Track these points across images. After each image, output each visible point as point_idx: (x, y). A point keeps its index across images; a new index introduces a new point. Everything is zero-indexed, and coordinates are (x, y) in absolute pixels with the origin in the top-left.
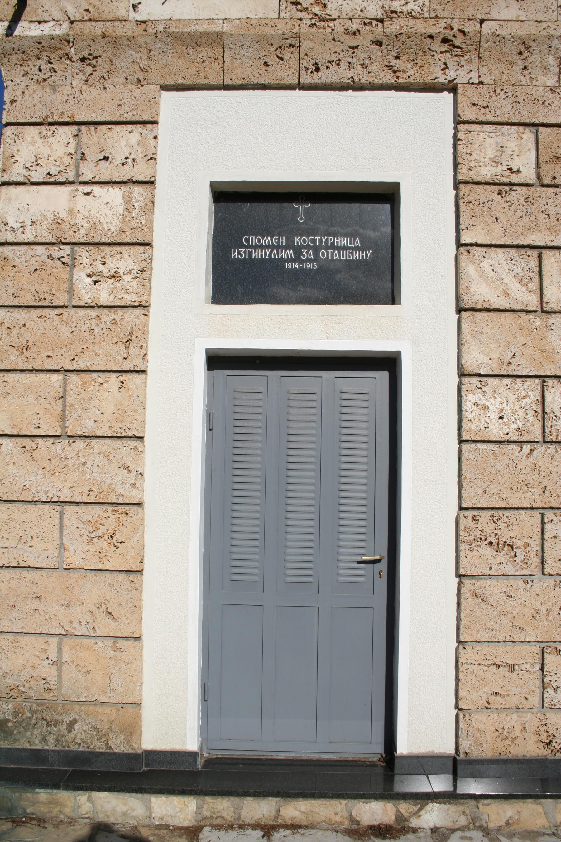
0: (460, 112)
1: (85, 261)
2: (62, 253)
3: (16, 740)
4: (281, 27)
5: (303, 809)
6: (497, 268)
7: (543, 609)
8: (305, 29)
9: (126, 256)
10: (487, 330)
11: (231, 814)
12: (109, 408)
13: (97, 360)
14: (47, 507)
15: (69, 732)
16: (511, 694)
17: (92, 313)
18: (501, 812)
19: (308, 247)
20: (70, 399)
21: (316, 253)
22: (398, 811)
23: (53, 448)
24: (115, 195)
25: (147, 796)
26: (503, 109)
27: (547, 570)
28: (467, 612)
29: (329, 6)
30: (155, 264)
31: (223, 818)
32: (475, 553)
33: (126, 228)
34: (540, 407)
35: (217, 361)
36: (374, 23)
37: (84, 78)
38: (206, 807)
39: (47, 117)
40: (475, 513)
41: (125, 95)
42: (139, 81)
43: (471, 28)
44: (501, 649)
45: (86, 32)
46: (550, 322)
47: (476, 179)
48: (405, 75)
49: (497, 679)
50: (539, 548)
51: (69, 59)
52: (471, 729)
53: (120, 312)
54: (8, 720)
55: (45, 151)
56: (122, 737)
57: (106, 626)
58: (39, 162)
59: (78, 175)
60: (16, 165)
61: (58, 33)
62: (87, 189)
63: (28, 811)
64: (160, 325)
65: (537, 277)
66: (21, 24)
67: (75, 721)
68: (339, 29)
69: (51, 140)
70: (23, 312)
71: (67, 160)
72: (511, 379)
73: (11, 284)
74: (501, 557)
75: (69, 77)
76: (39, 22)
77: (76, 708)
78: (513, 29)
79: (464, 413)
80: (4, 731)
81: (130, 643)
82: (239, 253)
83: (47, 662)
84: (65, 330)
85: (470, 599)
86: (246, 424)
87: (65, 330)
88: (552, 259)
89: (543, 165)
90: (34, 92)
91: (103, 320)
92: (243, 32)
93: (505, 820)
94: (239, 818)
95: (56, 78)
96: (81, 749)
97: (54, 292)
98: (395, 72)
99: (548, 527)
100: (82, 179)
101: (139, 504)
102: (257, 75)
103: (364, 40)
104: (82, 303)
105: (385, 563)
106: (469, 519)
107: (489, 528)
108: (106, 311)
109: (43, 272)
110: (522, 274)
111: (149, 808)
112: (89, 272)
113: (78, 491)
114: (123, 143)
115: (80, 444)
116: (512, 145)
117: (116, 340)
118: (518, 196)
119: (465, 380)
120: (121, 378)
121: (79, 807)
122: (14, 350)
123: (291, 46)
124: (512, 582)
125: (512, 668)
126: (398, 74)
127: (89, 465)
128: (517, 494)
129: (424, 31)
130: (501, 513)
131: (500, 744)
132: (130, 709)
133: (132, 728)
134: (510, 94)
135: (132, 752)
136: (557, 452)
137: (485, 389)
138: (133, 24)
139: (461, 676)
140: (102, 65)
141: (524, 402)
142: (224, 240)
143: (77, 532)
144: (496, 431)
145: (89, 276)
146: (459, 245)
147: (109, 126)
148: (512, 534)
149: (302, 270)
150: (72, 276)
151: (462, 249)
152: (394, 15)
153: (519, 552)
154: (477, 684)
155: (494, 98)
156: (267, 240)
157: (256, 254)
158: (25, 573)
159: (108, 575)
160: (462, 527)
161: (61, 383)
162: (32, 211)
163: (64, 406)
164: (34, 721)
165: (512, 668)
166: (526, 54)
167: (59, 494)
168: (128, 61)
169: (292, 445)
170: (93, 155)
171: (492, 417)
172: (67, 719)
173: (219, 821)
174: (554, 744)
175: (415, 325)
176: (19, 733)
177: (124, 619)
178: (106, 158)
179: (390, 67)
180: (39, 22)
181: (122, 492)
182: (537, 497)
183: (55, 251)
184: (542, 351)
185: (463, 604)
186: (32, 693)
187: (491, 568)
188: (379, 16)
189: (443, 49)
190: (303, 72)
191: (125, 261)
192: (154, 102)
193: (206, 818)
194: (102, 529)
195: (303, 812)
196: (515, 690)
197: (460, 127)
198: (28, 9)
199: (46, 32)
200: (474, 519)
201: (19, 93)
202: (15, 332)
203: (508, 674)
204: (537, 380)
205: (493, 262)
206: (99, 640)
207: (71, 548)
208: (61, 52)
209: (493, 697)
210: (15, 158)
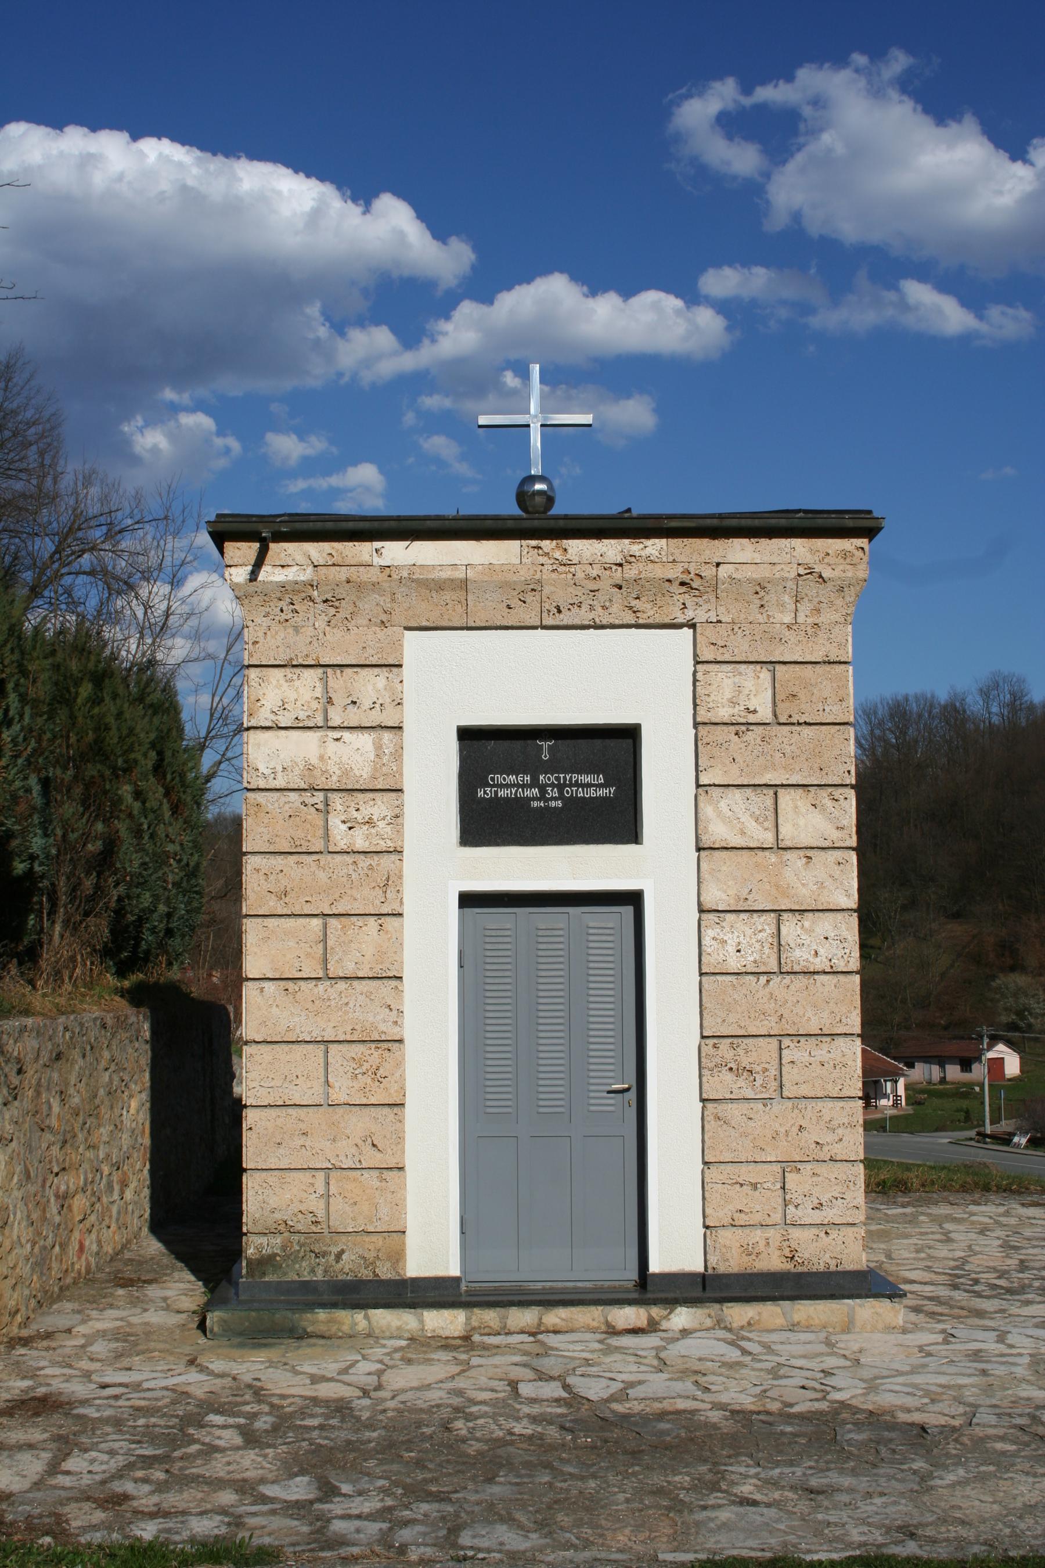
0: (698, 652)
1: (339, 807)
2: (315, 800)
3: (285, 1274)
4: (524, 574)
5: (563, 1316)
7: (782, 1130)
8: (547, 575)
10: (724, 868)
11: (498, 1323)
13: (356, 905)
14: (311, 1046)
15: (337, 1262)
16: (754, 1210)
17: (349, 859)
19: (553, 785)
20: (330, 943)
21: (561, 792)
23: (316, 990)
24: (365, 741)
25: (419, 1311)
26: (741, 648)
27: (785, 1094)
28: (711, 1134)
29: (570, 551)
30: (406, 809)
31: (490, 1327)
32: (716, 1078)
33: (378, 775)
34: (775, 940)
35: (468, 900)
36: (614, 567)
37: (326, 619)
38: (474, 1318)
39: (291, 659)
40: (715, 1041)
41: (369, 637)
43: (708, 572)
44: (744, 1168)
46: (785, 858)
47: (714, 720)
48: (645, 616)
49: (740, 1198)
50: (777, 1073)
52: (717, 1245)
53: (376, 857)
54: (277, 1254)
55: (291, 695)
56: (388, 1265)
58: (286, 706)
59: (326, 720)
60: (262, 710)
61: (302, 578)
62: (337, 734)
63: (309, 1330)
64: (414, 870)
65: (773, 815)
66: (265, 568)
67: (343, 1252)
69: (297, 683)
70: (280, 859)
71: (315, 705)
72: (748, 914)
73: (265, 830)
74: (741, 1082)
75: (312, 618)
77: (344, 1238)
78: (749, 572)
79: (703, 947)
80: (273, 1266)
81: (395, 1172)
82: (485, 792)
83: (315, 1195)
84: (322, 876)
85: (713, 1122)
86: (496, 960)
88: (788, 797)
89: (778, 703)
90: (277, 633)
91: (360, 866)
93: (747, 1320)
94: (505, 1326)
95: (298, 619)
96: (349, 1278)
97: (309, 838)
98: (634, 612)
99: (784, 1052)
100: (330, 724)
101: (400, 1041)
102: (500, 617)
103: (605, 585)
104: (338, 849)
105: (634, 1090)
106: (710, 1046)
107: (729, 1055)
108: (362, 857)
109: (298, 819)
110: (758, 813)
111: (422, 1322)
112: (343, 818)
113: (341, 1030)
114: (370, 688)
115: (342, 985)
116: (749, 684)
117: (374, 884)
119: (705, 916)
120: (380, 921)
121: (356, 1324)
122: (273, 896)
124: (752, 1105)
125: (754, 1186)
127: (351, 1005)
128: (755, 1023)
130: (740, 1040)
131: (746, 1259)
133: (398, 1256)
134: (747, 632)
135: (397, 1278)
137: (724, 924)
138: (377, 570)
139: (707, 1195)
140: (346, 608)
141: (760, 936)
142: (470, 779)
143: (341, 1069)
144: (734, 964)
145: (344, 822)
146: (698, 786)
147: (355, 670)
149: (547, 808)
151: (700, 790)
152: (633, 559)
153: (758, 1077)
154: (722, 1202)
155: (732, 637)
156: (512, 778)
157: (502, 793)
158: (290, 1110)
159: (373, 1109)
160: (703, 1054)
162: (282, 756)
164: (302, 1254)
165: (754, 1186)
166: (762, 593)
167: (323, 1033)
168: (370, 604)
169: (541, 980)
170: (340, 699)
172: (335, 1250)
173: (486, 1330)
174: (796, 1258)
175: (657, 864)
176: (288, 1266)
177: (389, 1150)
178: (354, 703)
179: (631, 608)
180: (283, 566)
181: (385, 1029)
182: (774, 1024)
183: (307, 797)
184: (777, 887)
185: (707, 1127)
186: (299, 1227)
190: (545, 614)
191: (379, 808)
192: (397, 645)
193: (474, 1329)
194: (366, 1066)
195: (563, 1320)
196: (758, 1208)
197: (699, 666)
198: (270, 553)
199: (290, 578)
200: (715, 1046)
201: (261, 634)
202: (272, 878)
203: (750, 1192)
204: (772, 915)
205: (730, 802)
206: (363, 1172)
207: (337, 1085)
208: (303, 595)
209: (738, 1214)
210: (262, 702)
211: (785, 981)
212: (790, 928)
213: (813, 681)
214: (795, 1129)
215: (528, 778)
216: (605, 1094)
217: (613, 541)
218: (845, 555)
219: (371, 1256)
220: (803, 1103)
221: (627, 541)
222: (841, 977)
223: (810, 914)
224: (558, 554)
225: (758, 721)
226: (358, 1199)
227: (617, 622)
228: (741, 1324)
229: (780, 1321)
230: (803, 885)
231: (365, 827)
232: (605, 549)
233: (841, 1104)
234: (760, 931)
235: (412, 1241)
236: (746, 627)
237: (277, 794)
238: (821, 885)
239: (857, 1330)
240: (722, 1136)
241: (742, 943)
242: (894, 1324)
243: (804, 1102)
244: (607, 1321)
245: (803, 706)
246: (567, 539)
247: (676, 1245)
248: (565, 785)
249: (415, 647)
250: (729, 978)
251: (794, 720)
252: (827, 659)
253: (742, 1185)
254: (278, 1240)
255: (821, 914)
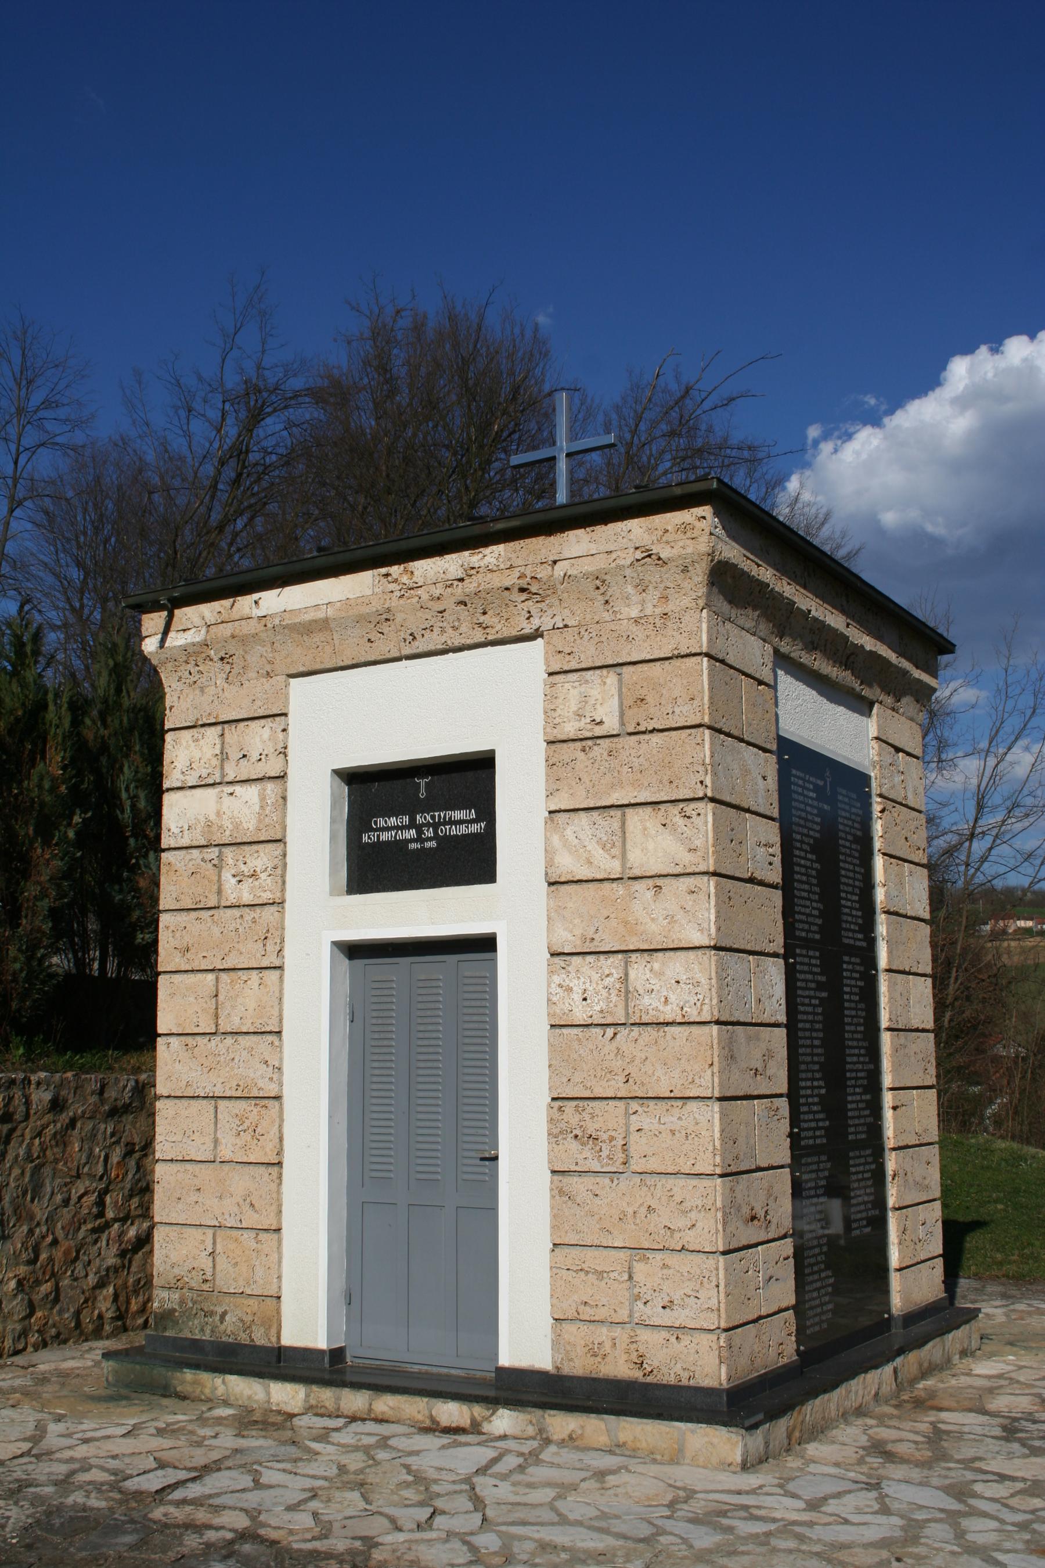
3: (181, 1331)
4: (376, 605)
5: (391, 1404)
6: (581, 836)
7: (630, 1211)
9: (262, 854)
12: (252, 1005)
15: (222, 1323)
17: (236, 912)
18: (564, 1424)
19: (428, 825)
20: (221, 997)
21: (435, 832)
22: (472, 1414)
24: (250, 793)
25: (266, 1381)
26: (588, 655)
29: (416, 573)
33: (261, 826)
35: (355, 951)
36: (456, 583)
38: (312, 1395)
42: (268, 673)
43: (543, 573)
44: (590, 1253)
45: (219, 635)
46: (633, 889)
48: (493, 631)
51: (211, 660)
53: (258, 909)
54: (175, 1310)
57: (251, 1219)
59: (223, 776)
61: (198, 640)
62: (230, 789)
66: (172, 634)
67: (225, 1313)
68: (425, 597)
75: (213, 677)
76: (184, 630)
78: (589, 566)
82: (369, 838)
84: (216, 931)
87: (216, 931)
92: (344, 614)
93: (567, 1433)
94: (339, 1409)
102: (364, 653)
104: (229, 904)
108: (247, 910)
111: (268, 1393)
112: (233, 872)
114: (258, 739)
115: (229, 1040)
117: (256, 938)
118: (601, 751)
121: (216, 1389)
123: (387, 620)
124: (598, 1180)
126: (488, 630)
127: (236, 1060)
129: (499, 585)
130: (586, 1103)
131: (592, 1360)
132: (271, 1302)
133: (274, 1321)
134: (594, 634)
135: (269, 1345)
136: (640, 1034)
138: (255, 620)
142: (358, 821)
143: (227, 1126)
145: (234, 876)
148: (597, 1126)
149: (423, 848)
150: (220, 876)
152: (473, 572)
153: (604, 1146)
155: (579, 641)
157: (385, 836)
158: (188, 1166)
161: (214, 982)
163: (217, 1003)
164: (194, 1311)
167: (215, 1089)
168: (256, 656)
170: (234, 754)
171: (576, 999)
172: (220, 1310)
173: (322, 1411)
174: (645, 1365)
175: (508, 907)
176: (183, 1322)
179: (480, 624)
180: (184, 630)
184: (626, 923)
187: (577, 1164)
188: (460, 575)
189: (523, 599)
191: (261, 859)
194: (247, 1123)
196: (604, 1301)
198: (175, 619)
199: (189, 641)
202: (178, 934)
205: (576, 829)
208: (204, 655)
211: (633, 1034)
212: (640, 971)
213: (662, 681)
214: (643, 1210)
215: (406, 819)
216: (478, 1162)
217: (454, 556)
218: (685, 528)
219: (248, 1319)
220: (650, 1180)
221: (466, 553)
222: (694, 1029)
223: (660, 954)
224: (405, 579)
225: (605, 733)
226: (238, 1260)
227: (469, 642)
228: (561, 1437)
229: (603, 1440)
230: (653, 919)
231: (250, 880)
232: (447, 565)
233: (694, 1182)
234: (608, 976)
235: (288, 1308)
236: (594, 629)
237: (183, 852)
238: (671, 918)
239: (687, 1461)
240: (567, 1214)
241: (592, 988)
242: (730, 1460)
243: (656, 1177)
244: (431, 1415)
245: (652, 710)
246: (413, 561)
247: (525, 1339)
248: (440, 824)
249: (302, 694)
250: (575, 1031)
251: (642, 728)
252: (676, 652)
253: (587, 1272)
254: (176, 1296)
255: (672, 953)
